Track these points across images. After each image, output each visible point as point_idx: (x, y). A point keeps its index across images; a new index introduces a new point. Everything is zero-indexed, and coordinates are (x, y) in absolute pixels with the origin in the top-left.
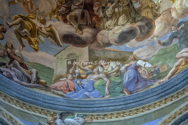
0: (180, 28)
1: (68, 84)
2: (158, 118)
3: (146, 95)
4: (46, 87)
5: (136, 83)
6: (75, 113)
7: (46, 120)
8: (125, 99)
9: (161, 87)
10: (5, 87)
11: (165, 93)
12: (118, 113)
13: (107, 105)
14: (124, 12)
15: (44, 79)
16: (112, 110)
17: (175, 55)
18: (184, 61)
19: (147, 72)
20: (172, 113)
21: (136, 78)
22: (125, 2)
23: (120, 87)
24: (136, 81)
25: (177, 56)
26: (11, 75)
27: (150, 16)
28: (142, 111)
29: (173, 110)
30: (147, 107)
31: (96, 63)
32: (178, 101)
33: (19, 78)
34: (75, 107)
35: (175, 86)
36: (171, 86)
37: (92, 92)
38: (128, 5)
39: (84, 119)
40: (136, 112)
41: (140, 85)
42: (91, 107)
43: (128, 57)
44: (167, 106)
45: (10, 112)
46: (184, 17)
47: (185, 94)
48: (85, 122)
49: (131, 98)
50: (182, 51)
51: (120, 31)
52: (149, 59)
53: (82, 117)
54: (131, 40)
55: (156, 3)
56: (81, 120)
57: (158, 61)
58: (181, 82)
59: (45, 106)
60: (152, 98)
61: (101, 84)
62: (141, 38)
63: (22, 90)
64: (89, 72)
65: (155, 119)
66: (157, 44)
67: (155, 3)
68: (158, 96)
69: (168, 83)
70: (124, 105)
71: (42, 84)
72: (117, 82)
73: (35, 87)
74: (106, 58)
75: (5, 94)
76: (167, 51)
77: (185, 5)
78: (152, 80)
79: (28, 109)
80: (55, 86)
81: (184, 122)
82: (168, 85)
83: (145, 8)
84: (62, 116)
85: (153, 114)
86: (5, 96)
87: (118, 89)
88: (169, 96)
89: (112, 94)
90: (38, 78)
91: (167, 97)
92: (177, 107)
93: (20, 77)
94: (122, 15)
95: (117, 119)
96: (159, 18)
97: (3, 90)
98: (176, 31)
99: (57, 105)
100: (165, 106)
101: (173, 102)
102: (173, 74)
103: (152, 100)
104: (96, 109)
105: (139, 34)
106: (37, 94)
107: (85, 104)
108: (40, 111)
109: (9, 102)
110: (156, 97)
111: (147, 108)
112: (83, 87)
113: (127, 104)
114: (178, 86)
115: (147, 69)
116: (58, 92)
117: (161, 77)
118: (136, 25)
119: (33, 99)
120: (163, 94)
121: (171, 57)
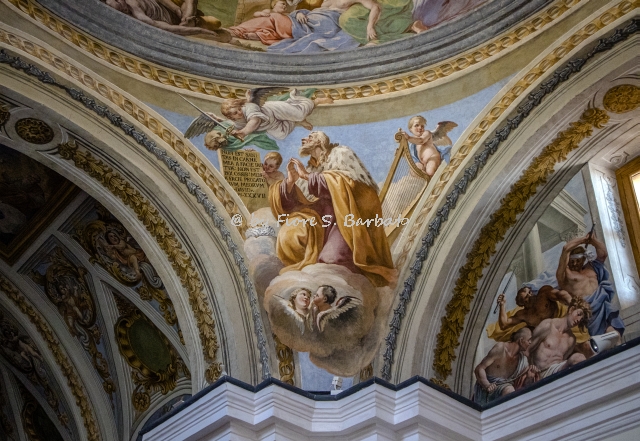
1: (273, 23)
2: (498, 80)
4: (217, 31)
6: (291, 88)
7: (218, 107)
8: (413, 41)
10: (110, 30)
11: (515, 14)
12: (398, 81)
13: (368, 62)
15: (213, 15)
16: (383, 74)
20: (535, 63)
23: (403, 18)
26: (128, 6)
28: (458, 69)
30: (470, 57)
32: (550, 28)
33: (149, 12)
34: (290, 73)
37: (334, 36)
39: (313, 99)
40: (441, 71)
42: (328, 71)
44: (519, 47)
45: (126, 90)
48: (315, 107)
49: (429, 37)
53: (308, 96)
56: (306, 103)
59: (215, 74)
60: (481, 33)
61: (355, 17)
63: (155, 36)
65: (490, 85)
68: (498, 26)
70: (410, 57)
71: (209, 25)
72: (399, 8)
73: (191, 33)
75: (114, 48)
79: (173, 83)
80: (242, 30)
81: (568, 82)
84: (257, 97)
85: (486, 73)
86: (113, 54)
87: (399, 23)
89: (384, 36)
90: (198, 14)
91: (522, 23)
92: (546, 46)
93: (152, 10)
95: (394, 94)
97: (107, 38)
99: (244, 70)
101: (536, 34)
103: (483, 37)
104: (341, 74)
106: (191, 46)
107: (314, 64)
108: (204, 86)
109: (124, 66)
111: (469, 60)
112: (311, 28)
113: (419, 54)
116: (250, 42)
119: (184, 58)
120: (511, 17)
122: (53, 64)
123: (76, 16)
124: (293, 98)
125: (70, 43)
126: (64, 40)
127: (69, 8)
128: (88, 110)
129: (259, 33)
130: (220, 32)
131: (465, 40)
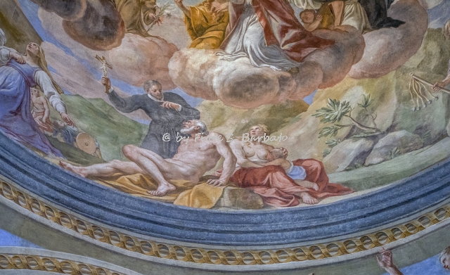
0: (168, 104)
2: (22, 237)
3: (34, 167)
5: (11, 112)
9: (76, 184)
17: (126, 143)
18: (138, 175)
21: (19, 101)
24: (14, 108)
25: (128, 149)
27: (126, 13)
29: (67, 252)
32: (90, 243)
36: (96, 201)
41: (16, 125)
46: (190, 94)
47: (111, 243)
50: (145, 151)
52: (65, 93)
54: (54, 13)
57: (80, 116)
58: (123, 214)
60: (37, 184)
62: (75, 32)
65: (14, 233)
66: (100, 82)
67: (155, 4)
69: (95, 190)
76: (111, 116)
77: (212, 78)
78: (48, 143)
82: (92, 194)
85: (20, 221)
88: (75, 214)
92: (77, 253)
96: (140, 38)
98: (155, 100)
100: (52, 226)
103: (35, 188)
105: (76, 19)
110: (48, 190)
115: (50, 107)
117: (71, 155)
120: (67, 198)
121: (115, 139)
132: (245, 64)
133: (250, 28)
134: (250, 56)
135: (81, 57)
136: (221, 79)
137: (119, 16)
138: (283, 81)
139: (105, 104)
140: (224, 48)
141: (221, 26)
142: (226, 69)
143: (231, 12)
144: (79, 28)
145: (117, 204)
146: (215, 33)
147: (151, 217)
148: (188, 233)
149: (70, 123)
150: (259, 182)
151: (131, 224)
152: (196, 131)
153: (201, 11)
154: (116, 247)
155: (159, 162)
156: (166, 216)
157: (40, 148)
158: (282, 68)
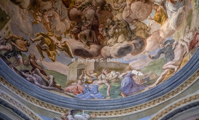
2: (148, 116)
4: (60, 89)
5: (131, 88)
6: (83, 110)
7: (60, 116)
10: (28, 89)
11: (153, 96)
13: (108, 105)
14: (123, 32)
15: (59, 84)
16: (112, 109)
17: (162, 66)
18: (169, 72)
19: (139, 80)
20: (159, 112)
21: (131, 83)
22: (123, 25)
23: (118, 90)
24: (131, 86)
25: (163, 67)
26: (33, 80)
27: (143, 36)
28: (135, 110)
30: (139, 107)
31: (101, 59)
33: (39, 82)
34: (83, 106)
35: (162, 90)
36: (158, 91)
37: (96, 94)
38: (126, 27)
39: (90, 115)
40: (130, 110)
41: (134, 89)
42: (95, 106)
43: (125, 67)
44: (155, 107)
45: (31, 109)
46: (169, 37)
48: (91, 118)
49: (127, 99)
51: (119, 47)
53: (88, 114)
55: (147, 25)
56: (88, 116)
57: (148, 71)
58: (167, 88)
59: (59, 104)
60: (143, 100)
62: (135, 53)
63: (42, 91)
64: (94, 78)
65: (145, 117)
66: (148, 58)
70: (121, 104)
71: (58, 87)
72: (116, 87)
73: (52, 89)
74: (108, 68)
75: (28, 95)
77: (171, 27)
78: (143, 86)
79: (46, 107)
82: (156, 90)
83: (139, 30)
84: (72, 113)
85: (144, 113)
86: (28, 97)
87: (117, 92)
90: (54, 83)
91: (155, 99)
92: (163, 108)
93: (40, 81)
94: (121, 34)
95: (116, 116)
96: (150, 37)
99: (69, 104)
101: (160, 103)
102: (160, 82)
103: (143, 101)
104: (99, 107)
108: (56, 108)
109: (31, 101)
111: (139, 108)
112: (89, 90)
113: (124, 104)
114: (164, 91)
116: (70, 93)
118: (131, 43)
119: (50, 99)
120: (152, 97)
121: (159, 68)
122: (9, 101)
123: (17, 84)
124: (84, 114)
125: (15, 93)
126: (13, 92)
127: (16, 82)
128: (18, 116)
129: (73, 91)
130: (61, 89)
131: (138, 101)
132: (174, 15)
133: (168, 6)
134: (174, 12)
135: (140, 57)
136: (173, 25)
137: (142, 38)
138: (184, 9)
139: (152, 62)
140: (168, 17)
141: (163, 13)
142: (172, 21)
143: (162, 7)
144: (135, 51)
145: (163, 86)
146: (163, 16)
147: (173, 82)
148: (185, 76)
149: (147, 75)
150: (195, 43)
151: (171, 88)
152: (176, 45)
153: (157, 15)
154: (171, 97)
155: (172, 63)
156: (176, 78)
157: (142, 89)
158: (182, 6)
